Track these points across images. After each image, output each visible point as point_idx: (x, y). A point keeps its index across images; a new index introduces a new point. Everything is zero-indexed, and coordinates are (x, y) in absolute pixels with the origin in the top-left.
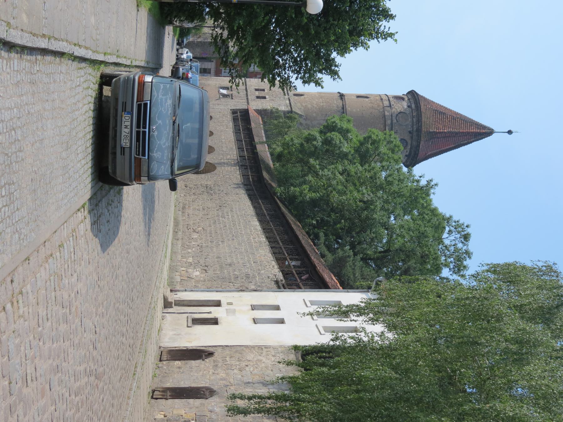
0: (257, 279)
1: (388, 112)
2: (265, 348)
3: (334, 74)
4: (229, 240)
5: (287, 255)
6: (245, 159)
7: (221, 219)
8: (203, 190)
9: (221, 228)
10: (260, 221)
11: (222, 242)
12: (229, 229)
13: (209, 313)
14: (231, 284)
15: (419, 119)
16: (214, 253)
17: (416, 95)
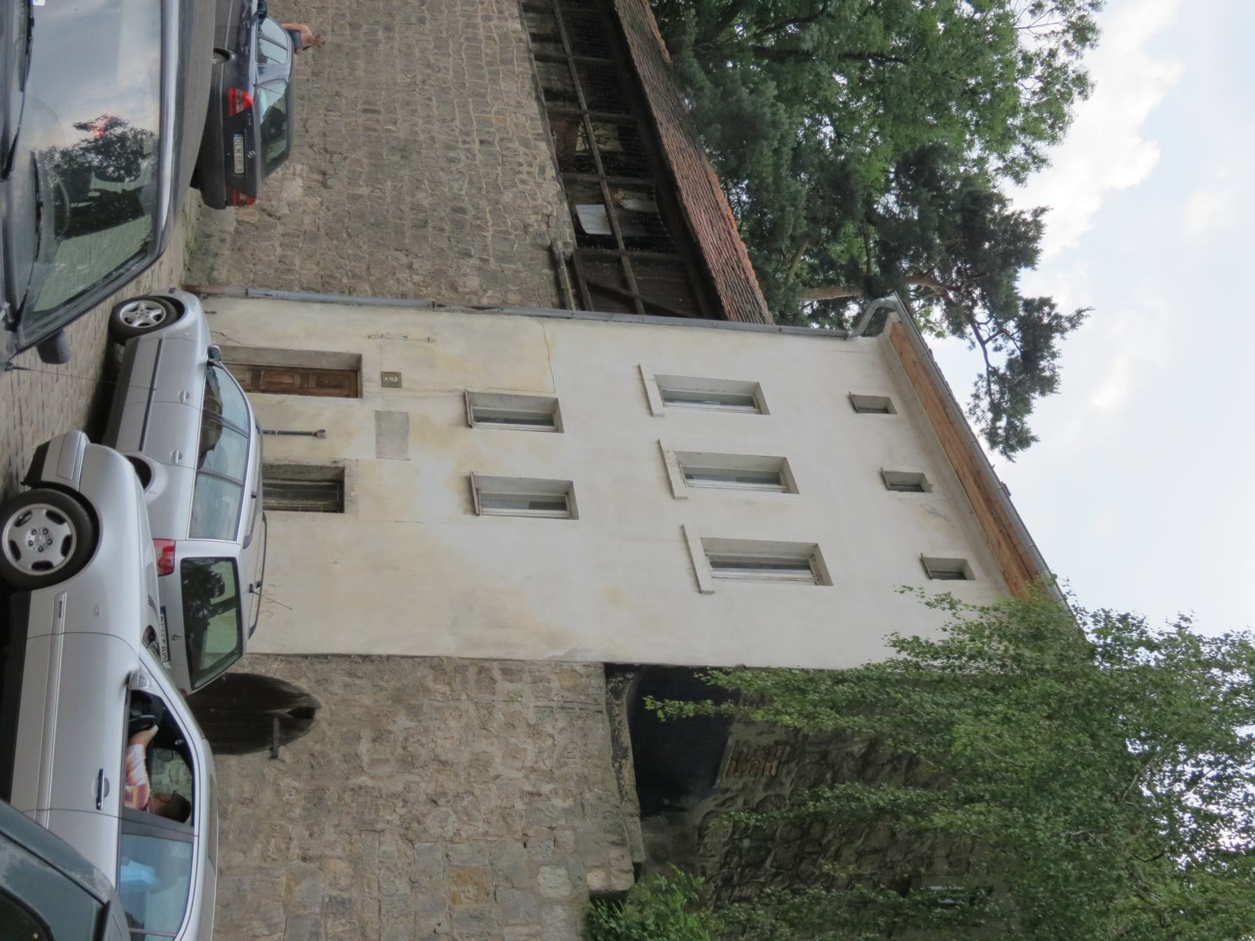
13: (315, 434)
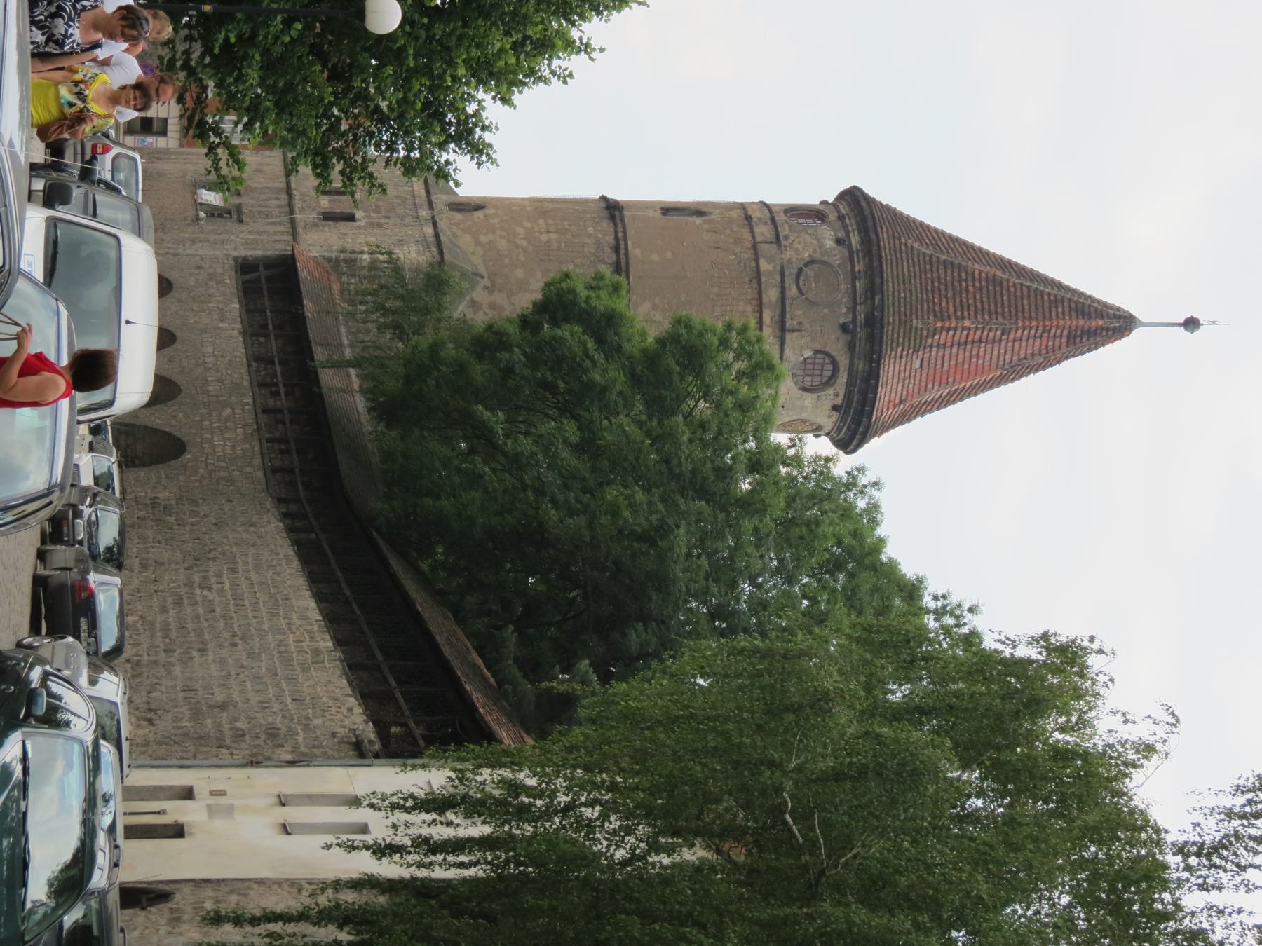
0: (300, 739)
1: (769, 262)
3: (479, 151)
4: (221, 646)
5: (394, 684)
6: (283, 422)
7: (198, 591)
8: (142, 513)
9: (198, 617)
10: (319, 597)
11: (200, 650)
12: (224, 617)
13: (159, 813)
14: (224, 751)
15: (872, 282)
16: (175, 679)
17: (864, 204)
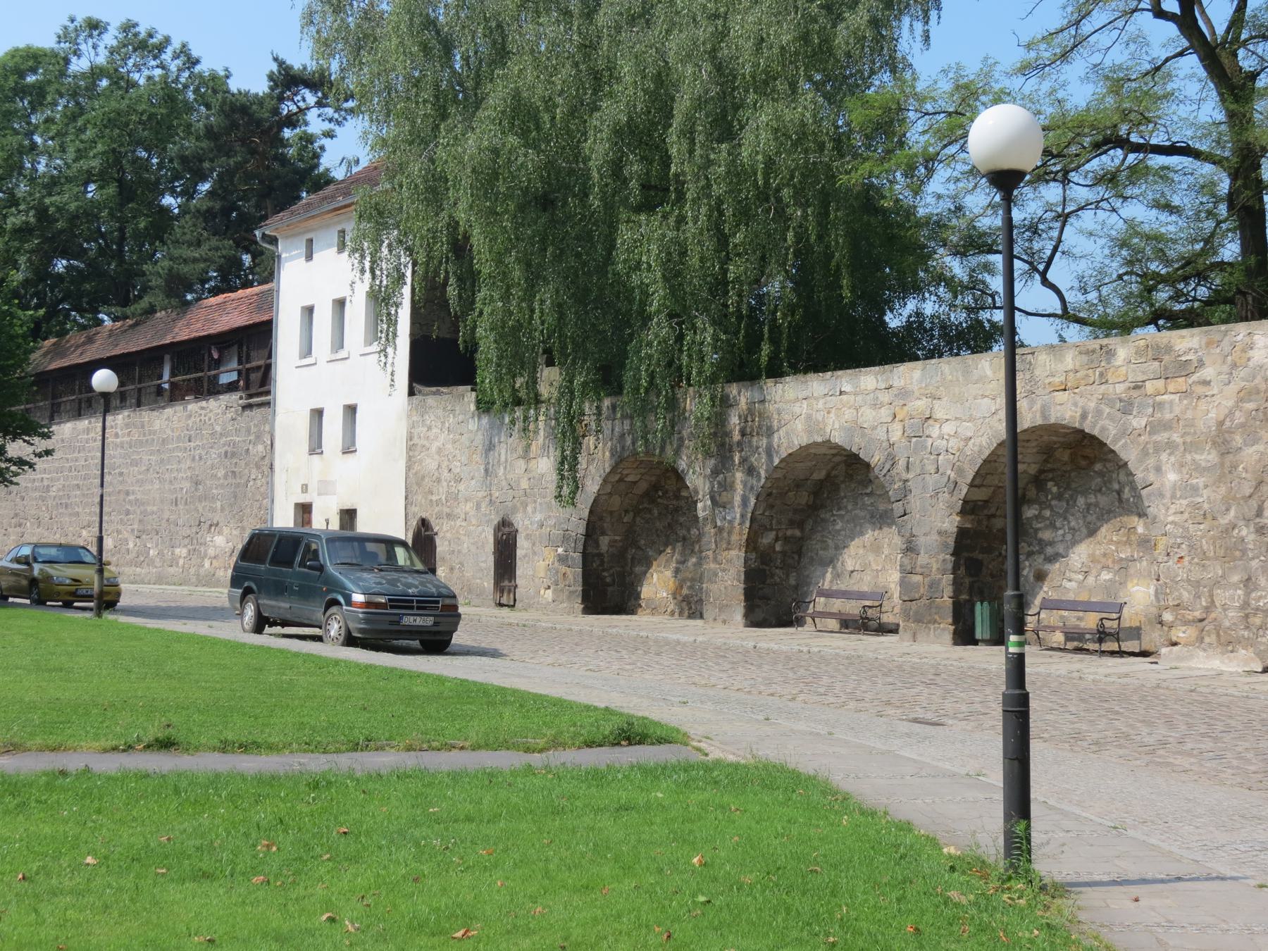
2: (411, 440)
